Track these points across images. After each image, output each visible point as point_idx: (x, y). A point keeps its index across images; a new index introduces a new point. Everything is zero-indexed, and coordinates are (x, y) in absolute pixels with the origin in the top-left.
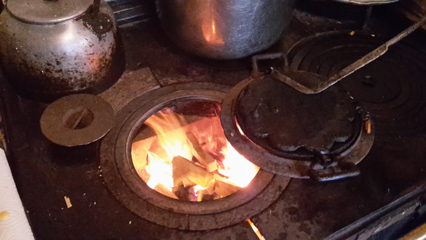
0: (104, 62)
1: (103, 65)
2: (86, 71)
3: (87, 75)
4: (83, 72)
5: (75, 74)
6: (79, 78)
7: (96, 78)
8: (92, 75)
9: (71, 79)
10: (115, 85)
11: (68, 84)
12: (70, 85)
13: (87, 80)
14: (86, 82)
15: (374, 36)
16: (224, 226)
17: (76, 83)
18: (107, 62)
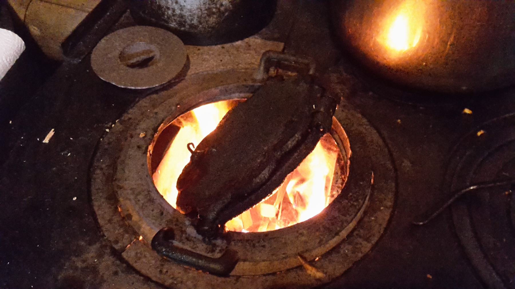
0: (218, 6)
1: (214, 10)
2: (189, 7)
3: (188, 13)
4: (184, 6)
5: (174, 4)
6: (178, 12)
7: (200, 23)
8: (196, 16)
9: (168, 8)
10: (227, 46)
11: (163, 14)
12: (166, 17)
13: (187, 20)
14: (185, 22)
15: (479, 134)
16: (160, 282)
17: (173, 18)
18: (222, 9)
